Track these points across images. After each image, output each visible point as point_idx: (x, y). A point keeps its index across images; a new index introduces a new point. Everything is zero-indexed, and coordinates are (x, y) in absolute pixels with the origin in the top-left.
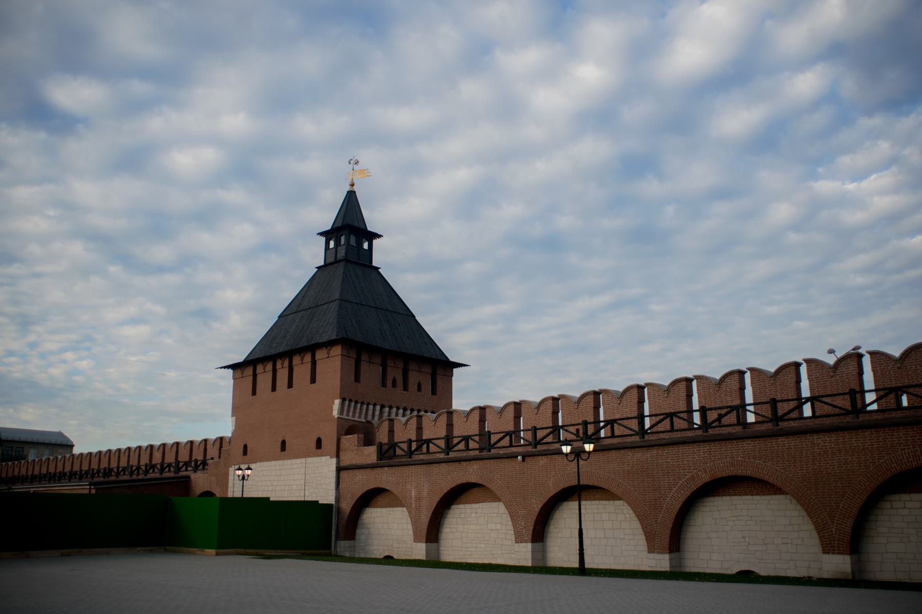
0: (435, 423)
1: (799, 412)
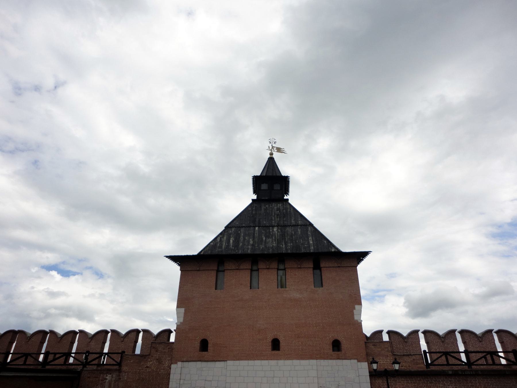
0: (91, 340)
1: (432, 358)
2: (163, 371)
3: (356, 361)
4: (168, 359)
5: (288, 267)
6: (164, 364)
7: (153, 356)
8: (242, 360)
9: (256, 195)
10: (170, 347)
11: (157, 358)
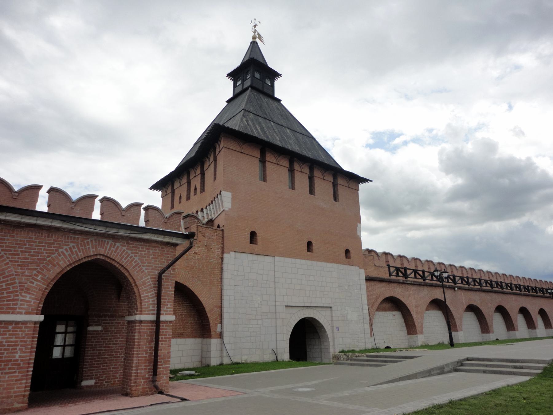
2: (213, 260)
3: (357, 268)
4: (217, 247)
5: (317, 176)
6: (213, 252)
7: (201, 242)
8: (286, 257)
9: (233, 81)
10: (218, 234)
11: (206, 245)
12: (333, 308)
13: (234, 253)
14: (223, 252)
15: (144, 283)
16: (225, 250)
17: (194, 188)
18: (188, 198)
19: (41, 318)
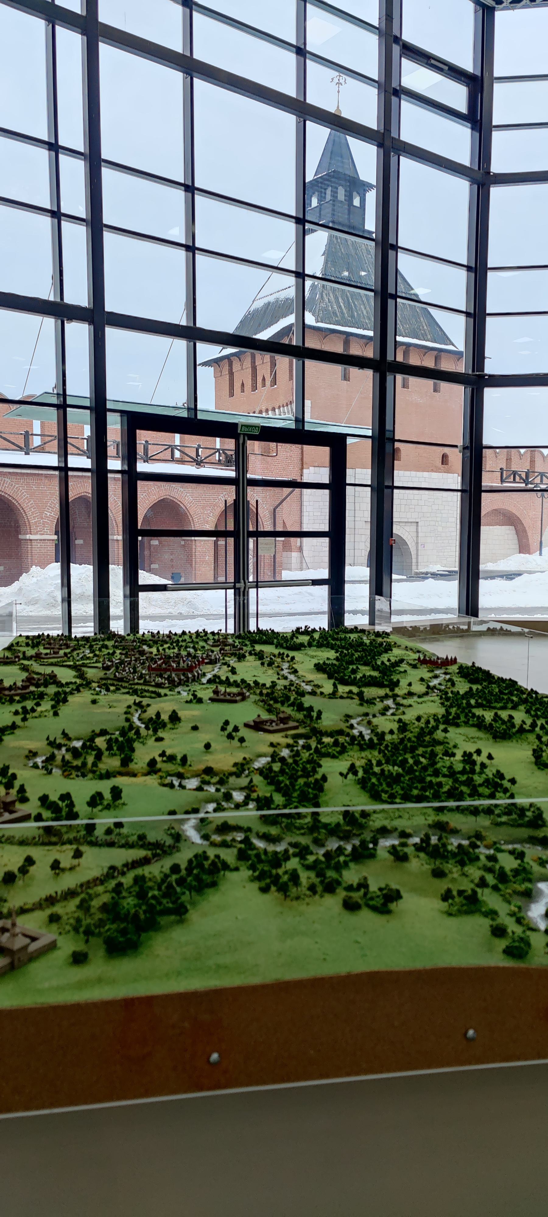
12: (420, 524)
13: (313, 468)
14: (302, 469)
15: (265, 516)
16: (304, 466)
17: (262, 378)
18: (254, 388)
19: (21, 537)
